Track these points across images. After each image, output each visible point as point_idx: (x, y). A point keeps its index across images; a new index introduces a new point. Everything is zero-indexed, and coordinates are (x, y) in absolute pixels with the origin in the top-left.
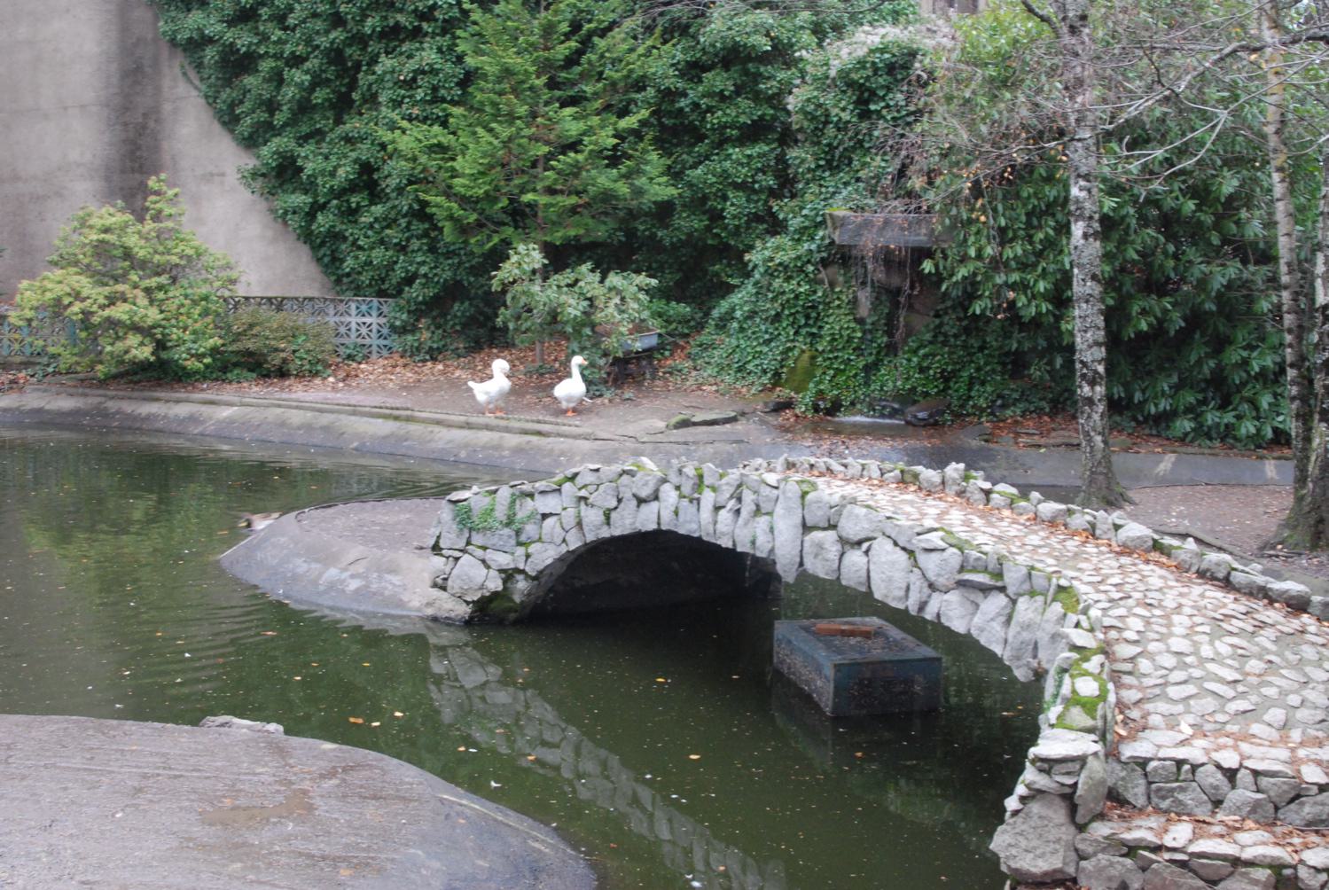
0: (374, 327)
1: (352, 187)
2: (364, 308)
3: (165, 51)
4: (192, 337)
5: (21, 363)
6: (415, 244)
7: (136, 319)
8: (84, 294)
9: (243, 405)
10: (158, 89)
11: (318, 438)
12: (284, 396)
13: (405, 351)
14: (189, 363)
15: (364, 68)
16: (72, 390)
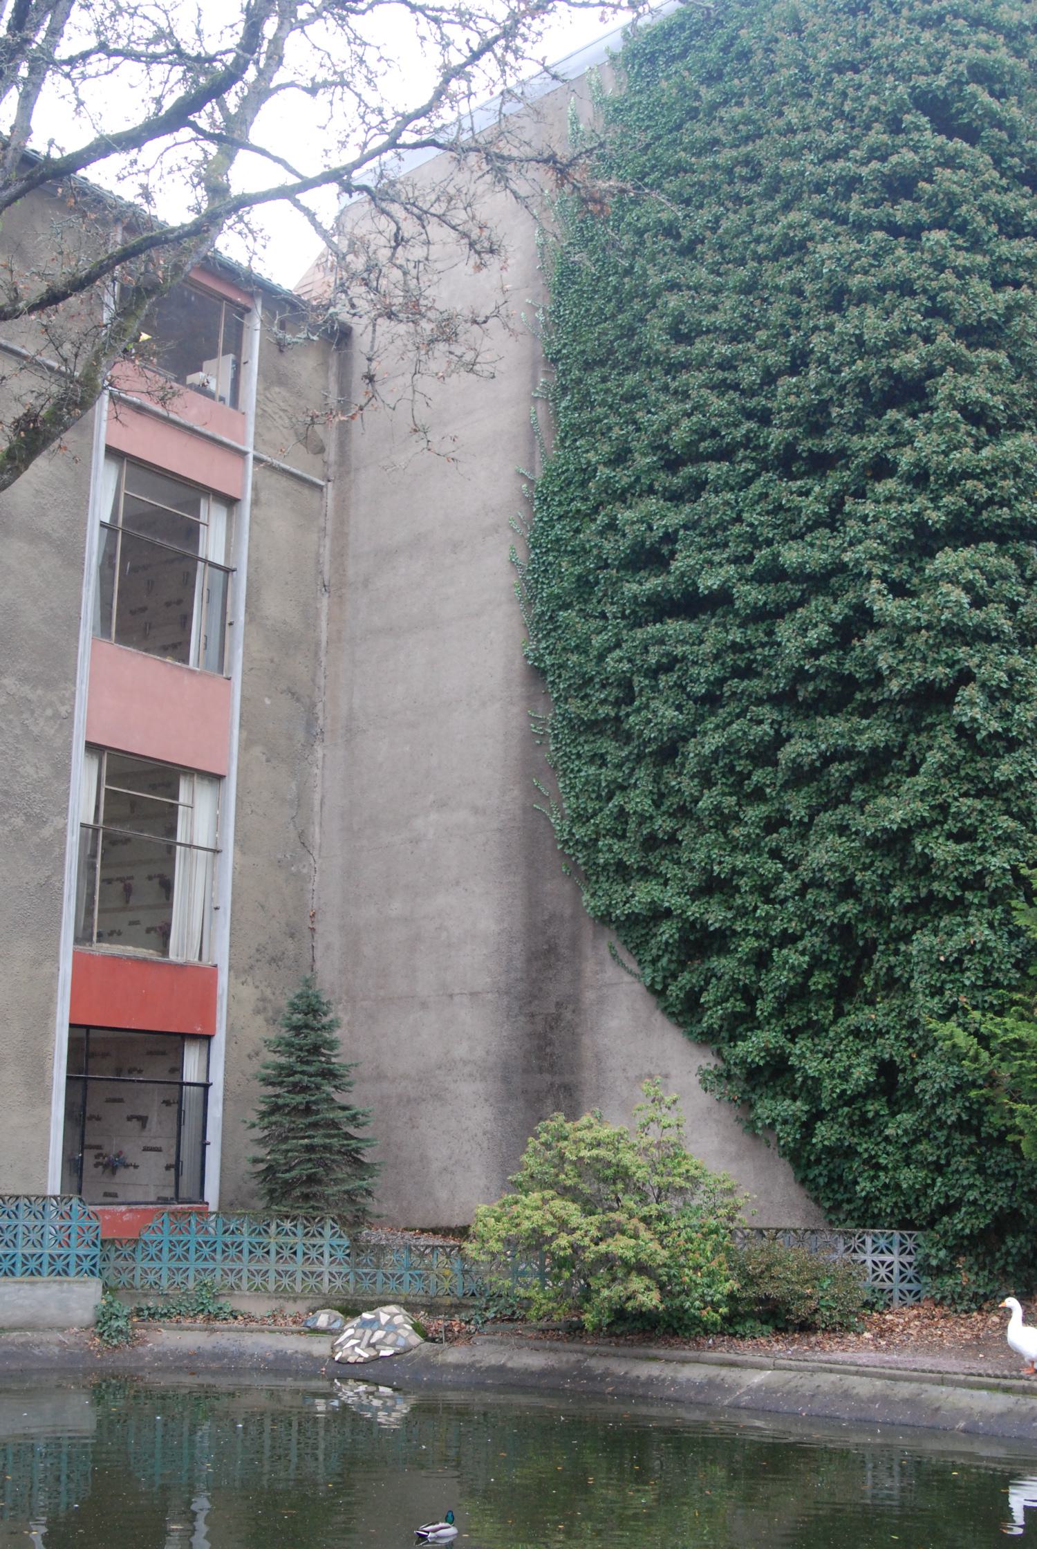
0: (896, 1267)
1: (869, 1092)
2: (882, 1242)
3: (588, 930)
4: (706, 1280)
5: (451, 1306)
6: (959, 1162)
7: (643, 1256)
8: (573, 1224)
9: (776, 1368)
10: (578, 974)
11: (905, 1416)
12: (824, 1357)
13: (943, 1298)
14: (704, 1312)
15: (881, 948)
16: (537, 1343)
